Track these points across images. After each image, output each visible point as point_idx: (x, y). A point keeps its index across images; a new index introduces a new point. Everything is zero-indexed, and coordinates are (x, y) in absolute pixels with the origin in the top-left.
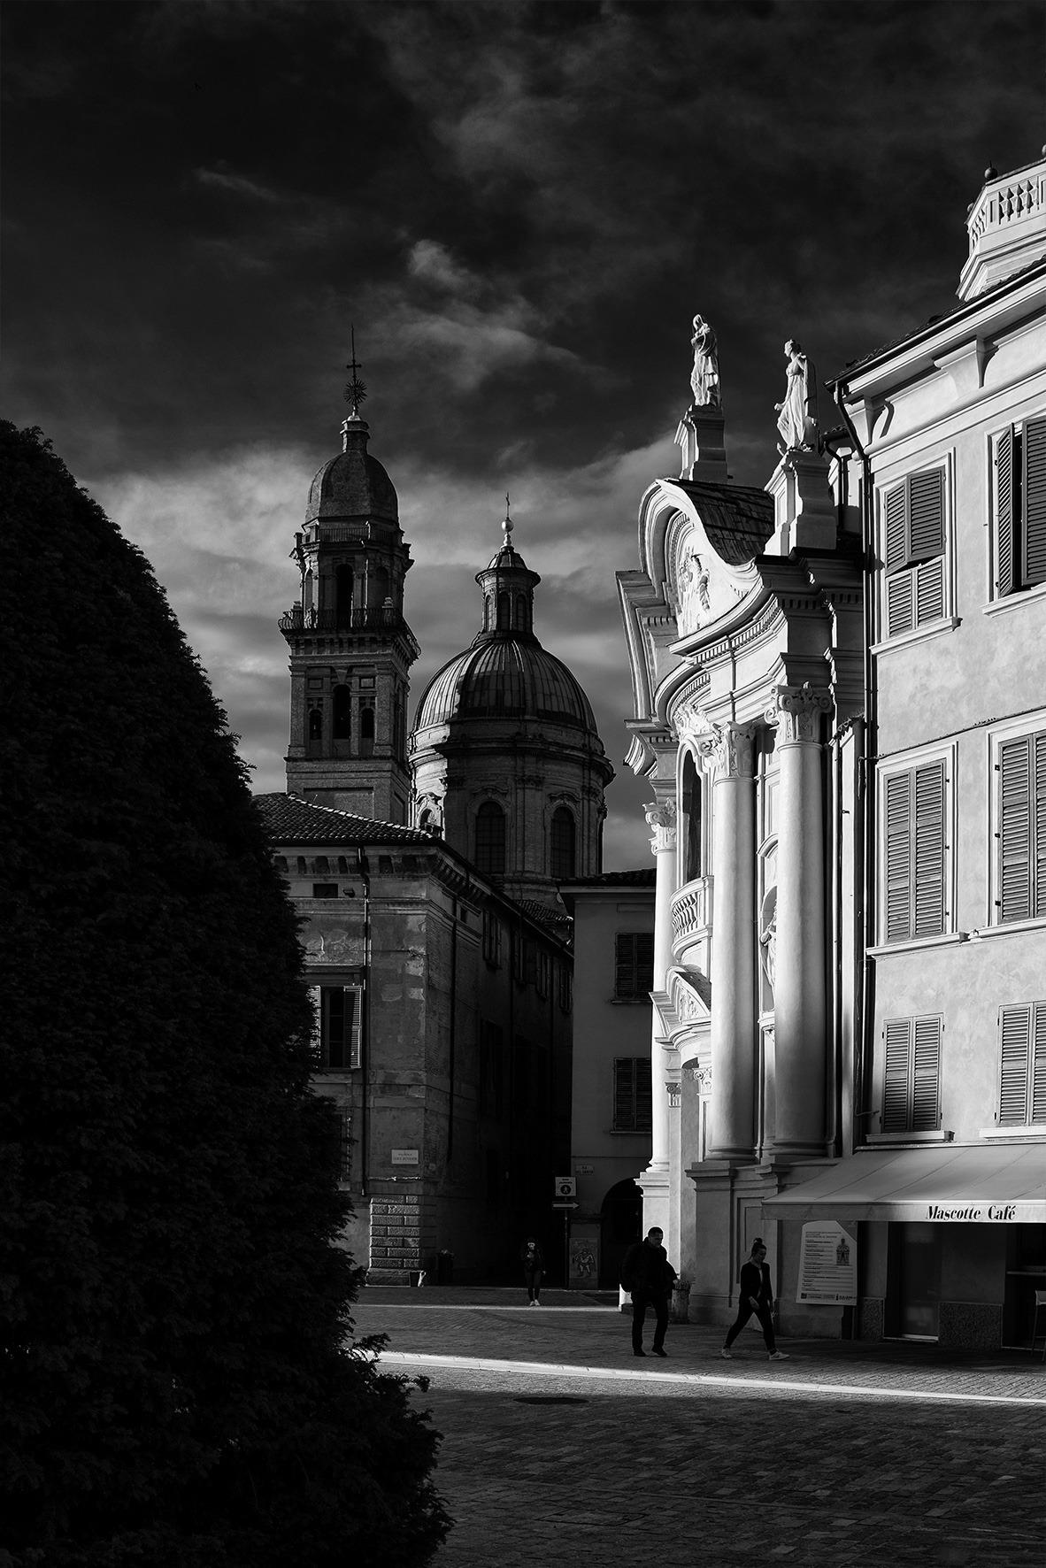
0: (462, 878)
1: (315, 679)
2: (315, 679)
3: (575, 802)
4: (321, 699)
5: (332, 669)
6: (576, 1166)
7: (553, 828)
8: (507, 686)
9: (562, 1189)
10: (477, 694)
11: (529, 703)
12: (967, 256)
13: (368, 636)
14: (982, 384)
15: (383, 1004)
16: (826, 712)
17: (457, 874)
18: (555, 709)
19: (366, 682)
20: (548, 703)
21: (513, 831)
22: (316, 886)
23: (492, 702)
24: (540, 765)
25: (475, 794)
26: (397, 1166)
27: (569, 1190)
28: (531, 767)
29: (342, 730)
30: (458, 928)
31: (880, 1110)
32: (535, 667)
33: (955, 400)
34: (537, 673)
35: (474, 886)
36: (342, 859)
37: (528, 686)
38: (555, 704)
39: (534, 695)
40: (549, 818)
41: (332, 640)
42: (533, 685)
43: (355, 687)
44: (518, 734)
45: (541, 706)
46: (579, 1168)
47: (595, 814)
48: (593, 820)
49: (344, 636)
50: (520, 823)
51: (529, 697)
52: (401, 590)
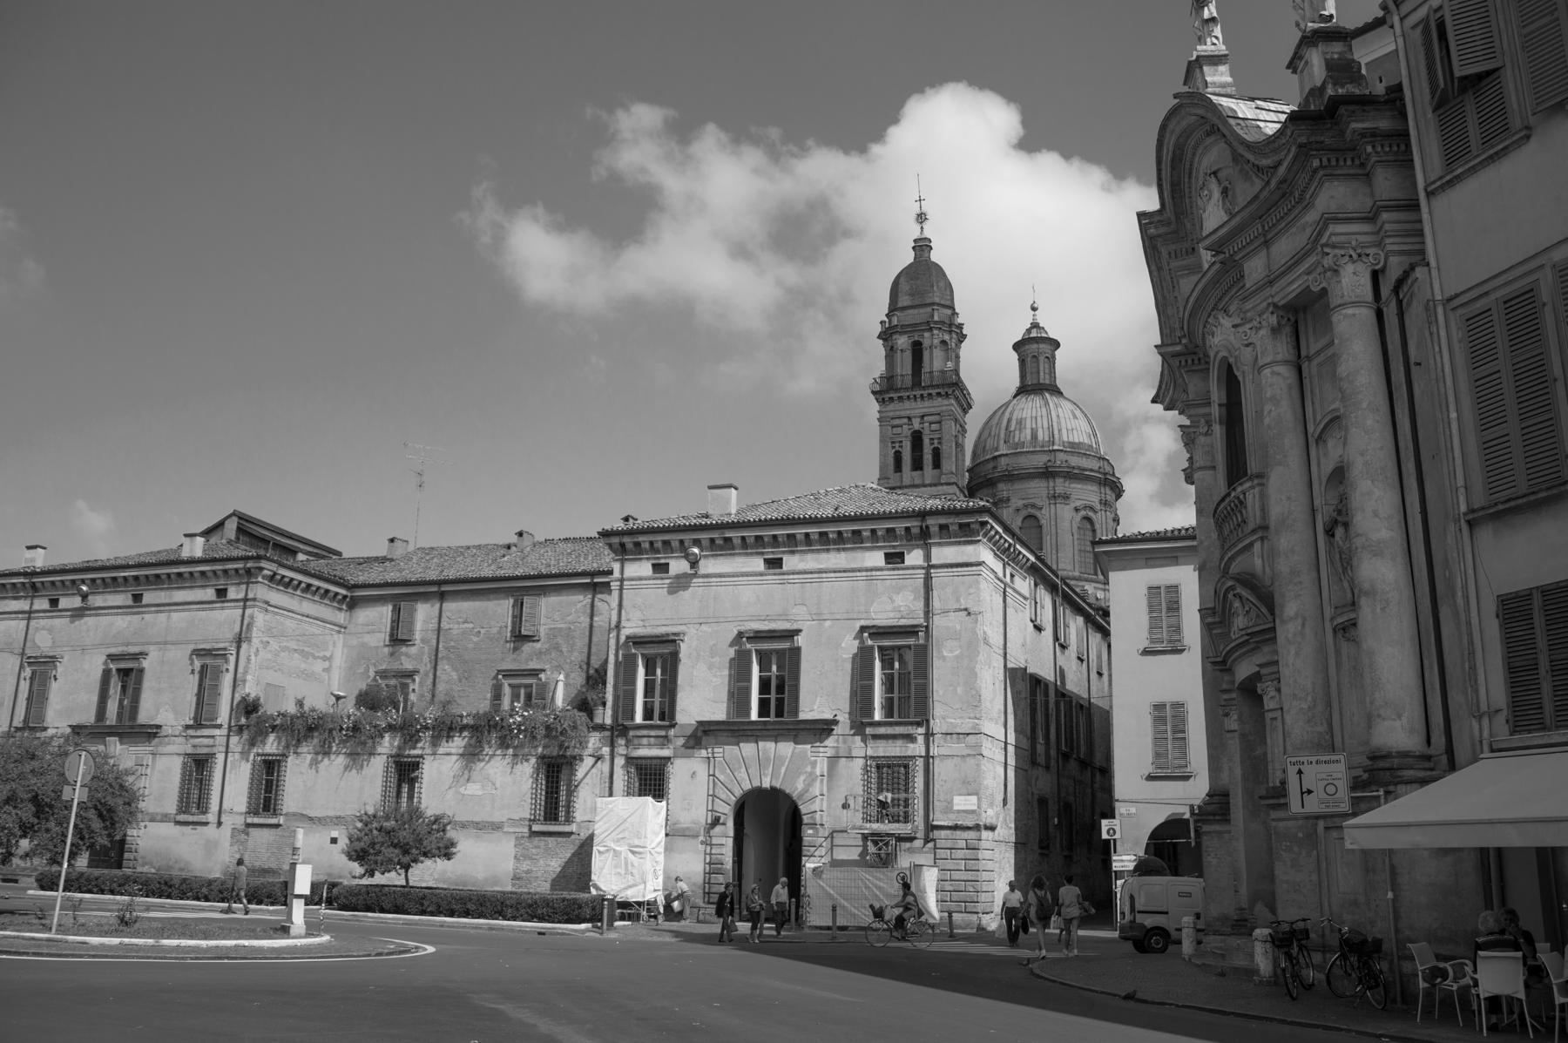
0: (1010, 545)
3: (1095, 512)
4: (901, 442)
5: (909, 418)
6: (1120, 809)
7: (1079, 534)
9: (1108, 832)
10: (1017, 433)
11: (1056, 436)
12: (1239, 382)
13: (934, 392)
15: (944, 658)
16: (1377, 268)
17: (1006, 540)
18: (1077, 441)
19: (934, 427)
20: (1071, 436)
21: (1049, 537)
22: (887, 555)
23: (1029, 437)
24: (1067, 485)
25: (1018, 510)
26: (959, 811)
27: (1115, 833)
28: (1060, 485)
29: (918, 465)
30: (1008, 589)
31: (1504, 706)
32: (1060, 410)
34: (1061, 415)
35: (1020, 552)
36: (907, 529)
37: (1055, 424)
38: (1076, 436)
39: (1060, 431)
40: (1075, 526)
41: (908, 397)
42: (1059, 423)
43: (926, 431)
44: (1049, 461)
45: (1065, 439)
46: (1123, 810)
47: (1111, 523)
48: (1110, 527)
49: (918, 393)
50: (1053, 531)
51: (1056, 432)
52: (958, 357)
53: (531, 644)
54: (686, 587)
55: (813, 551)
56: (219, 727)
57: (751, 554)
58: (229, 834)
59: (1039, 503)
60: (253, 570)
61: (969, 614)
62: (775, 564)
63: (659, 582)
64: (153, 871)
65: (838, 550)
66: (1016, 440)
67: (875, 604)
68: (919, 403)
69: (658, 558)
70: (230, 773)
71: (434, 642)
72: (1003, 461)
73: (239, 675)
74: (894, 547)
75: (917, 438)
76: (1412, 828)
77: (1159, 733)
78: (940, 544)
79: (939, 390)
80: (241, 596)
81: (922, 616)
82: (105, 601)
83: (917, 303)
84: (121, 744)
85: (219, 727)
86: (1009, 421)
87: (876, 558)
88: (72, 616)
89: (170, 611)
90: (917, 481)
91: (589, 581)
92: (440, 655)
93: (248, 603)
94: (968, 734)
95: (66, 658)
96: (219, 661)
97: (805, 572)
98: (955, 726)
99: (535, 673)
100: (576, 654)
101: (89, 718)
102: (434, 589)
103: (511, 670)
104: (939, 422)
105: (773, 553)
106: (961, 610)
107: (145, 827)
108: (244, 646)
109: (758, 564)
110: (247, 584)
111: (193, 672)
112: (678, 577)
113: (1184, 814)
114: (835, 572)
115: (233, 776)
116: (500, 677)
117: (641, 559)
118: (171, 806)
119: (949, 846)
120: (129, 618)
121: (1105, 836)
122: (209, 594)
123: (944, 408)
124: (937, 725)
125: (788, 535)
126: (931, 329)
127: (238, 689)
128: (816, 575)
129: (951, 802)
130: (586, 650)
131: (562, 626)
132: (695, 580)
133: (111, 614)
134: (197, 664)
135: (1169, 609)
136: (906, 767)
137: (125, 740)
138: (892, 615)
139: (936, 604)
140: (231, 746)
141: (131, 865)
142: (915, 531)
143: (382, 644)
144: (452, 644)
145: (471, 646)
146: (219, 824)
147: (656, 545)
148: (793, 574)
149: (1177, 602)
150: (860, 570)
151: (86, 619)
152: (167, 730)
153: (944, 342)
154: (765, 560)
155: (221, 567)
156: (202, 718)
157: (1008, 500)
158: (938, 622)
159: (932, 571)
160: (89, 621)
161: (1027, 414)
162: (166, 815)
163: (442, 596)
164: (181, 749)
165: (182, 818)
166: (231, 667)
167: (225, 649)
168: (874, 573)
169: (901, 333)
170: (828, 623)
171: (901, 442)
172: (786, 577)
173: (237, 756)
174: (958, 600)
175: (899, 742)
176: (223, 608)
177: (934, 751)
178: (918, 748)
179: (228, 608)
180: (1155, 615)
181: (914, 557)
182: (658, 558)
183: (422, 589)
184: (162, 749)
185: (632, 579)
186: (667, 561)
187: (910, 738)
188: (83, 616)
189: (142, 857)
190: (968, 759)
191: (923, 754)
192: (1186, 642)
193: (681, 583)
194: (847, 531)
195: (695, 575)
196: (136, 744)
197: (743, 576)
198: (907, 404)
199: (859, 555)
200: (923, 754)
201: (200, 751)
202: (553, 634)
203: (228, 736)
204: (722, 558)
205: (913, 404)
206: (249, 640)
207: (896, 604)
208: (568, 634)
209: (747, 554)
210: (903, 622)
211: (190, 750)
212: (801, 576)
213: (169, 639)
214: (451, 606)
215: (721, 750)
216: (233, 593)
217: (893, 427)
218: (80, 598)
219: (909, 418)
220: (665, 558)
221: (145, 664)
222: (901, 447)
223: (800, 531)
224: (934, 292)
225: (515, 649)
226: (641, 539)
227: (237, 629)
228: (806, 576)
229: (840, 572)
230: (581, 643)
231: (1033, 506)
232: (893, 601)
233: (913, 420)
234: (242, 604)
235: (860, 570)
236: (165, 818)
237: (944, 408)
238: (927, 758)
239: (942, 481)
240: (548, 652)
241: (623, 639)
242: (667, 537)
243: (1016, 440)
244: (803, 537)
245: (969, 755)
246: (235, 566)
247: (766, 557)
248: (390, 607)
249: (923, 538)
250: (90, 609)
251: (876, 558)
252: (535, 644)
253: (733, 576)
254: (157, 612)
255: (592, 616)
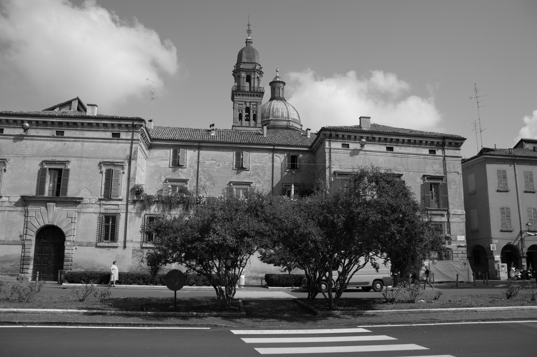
1: (241, 104)
2: (241, 104)
4: (242, 110)
5: (245, 102)
8: (284, 111)
10: (276, 113)
13: (255, 94)
14: (88, 105)
19: (254, 106)
26: (459, 241)
27: (494, 248)
29: (248, 120)
33: (48, 135)
36: (438, 142)
41: (246, 94)
43: (251, 108)
45: (292, 117)
53: (245, 171)
54: (357, 154)
55: (404, 146)
56: (121, 200)
57: (382, 144)
58: (131, 252)
60: (137, 126)
61: (458, 174)
62: (390, 149)
63: (346, 151)
64: (83, 270)
65: (413, 147)
66: (276, 115)
67: (427, 168)
68: (249, 98)
69: (345, 142)
70: (129, 222)
71: (196, 168)
72: (272, 122)
73: (131, 176)
74: (432, 148)
75: (248, 110)
77: (503, 217)
78: (448, 149)
79: (257, 94)
80: (129, 137)
81: (443, 173)
82: (38, 133)
83: (249, 61)
84: (56, 207)
85: (121, 200)
86: (273, 108)
87: (426, 151)
88: (14, 139)
89: (83, 141)
90: (248, 125)
91: (273, 148)
92: (199, 173)
93: (134, 142)
94: (461, 215)
95: (12, 161)
96: (118, 169)
97: (403, 153)
98: (457, 212)
99: (249, 184)
100: (266, 177)
101: (32, 192)
102: (197, 144)
103: (237, 182)
104: (257, 105)
105: (390, 145)
106: (456, 172)
107: (76, 249)
108: (133, 162)
109: (383, 148)
110: (133, 132)
111: (101, 172)
112: (354, 150)
113: (511, 242)
114: (413, 154)
115: (131, 224)
116: (232, 184)
117: (337, 141)
118: (93, 237)
119: (457, 253)
120: (55, 143)
121: (492, 249)
122: (109, 135)
123: (258, 101)
124: (452, 211)
125: (397, 139)
126: (255, 72)
127: (131, 182)
128: (406, 155)
129: (456, 238)
130: (271, 176)
131: (260, 165)
132: (361, 152)
133: (43, 140)
134: (104, 169)
135: (503, 178)
136: (441, 225)
137: (59, 205)
138: (433, 172)
140: (129, 209)
141: (69, 268)
142: (441, 143)
143: (168, 166)
144: (206, 169)
145: (215, 170)
146: (125, 247)
147: (345, 137)
148: (398, 153)
149: (506, 176)
150: (422, 155)
151: (24, 141)
152: (86, 201)
153: (258, 77)
154: (387, 147)
155: (118, 123)
156: (108, 195)
158: (449, 176)
159: (446, 158)
160: (26, 143)
161: (279, 107)
162: (90, 243)
163: (199, 148)
164: (97, 210)
165: (101, 244)
166: (126, 171)
167: (123, 163)
168: (426, 156)
169: (243, 71)
170: (411, 173)
171: (242, 110)
172: (395, 154)
173: (133, 215)
174: (454, 169)
175: (439, 217)
176: (118, 143)
177: (451, 220)
178: (445, 219)
179: (121, 143)
180: (500, 179)
181: (439, 152)
182: (345, 142)
183: (190, 144)
184: (83, 210)
185: (335, 149)
186: (348, 143)
187: (442, 215)
188: (22, 139)
189: (75, 264)
190: (461, 223)
191: (447, 221)
192: (509, 188)
193: (355, 152)
194: (418, 140)
195: (361, 150)
196: (67, 206)
197: (379, 152)
198: (245, 97)
199: (420, 149)
200: (447, 221)
201: (109, 212)
202: (255, 168)
203: (127, 205)
204: (370, 145)
206: (136, 159)
207: (434, 168)
208: (263, 168)
209: (380, 144)
210: (437, 175)
211: (103, 211)
212: (401, 155)
213: (84, 155)
214: (203, 153)
215: (40, 209)
216: (123, 135)
217: (239, 104)
218: (23, 130)
219: (245, 102)
220: (348, 142)
221: (69, 167)
222: (242, 112)
223: (401, 138)
224: (255, 59)
225: (237, 173)
226: (339, 133)
227: (128, 153)
228: (402, 155)
229: (415, 155)
230: (269, 173)
232: (433, 167)
233: (247, 103)
234: (130, 141)
235: (422, 155)
236: (89, 244)
237: (258, 101)
238: (449, 222)
239: (257, 126)
240: (253, 175)
241: (332, 172)
242: (350, 134)
243: (276, 115)
244: (402, 140)
245: (461, 222)
246: (127, 123)
247: (387, 146)
248: (172, 150)
249: (442, 146)
250: (28, 136)
251: (426, 151)
252: (247, 172)
253: (376, 152)
254: (75, 141)
255: (273, 162)
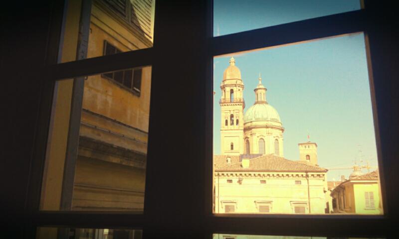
5: (230, 111)
13: (237, 104)
19: (237, 114)
29: (232, 124)
59: (264, 135)
68: (233, 107)
75: (232, 116)
76: (142, 133)
139: (311, 196)
142: (304, 175)
157: (255, 134)
205: (231, 107)
219: (230, 111)
231: (263, 136)
